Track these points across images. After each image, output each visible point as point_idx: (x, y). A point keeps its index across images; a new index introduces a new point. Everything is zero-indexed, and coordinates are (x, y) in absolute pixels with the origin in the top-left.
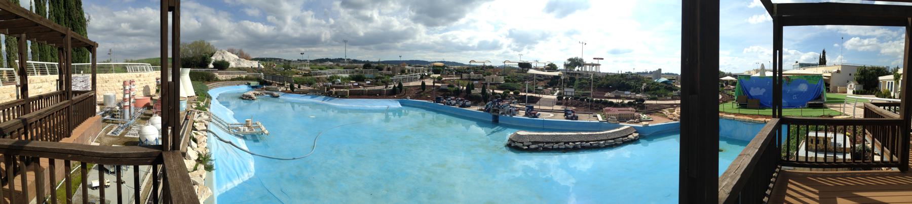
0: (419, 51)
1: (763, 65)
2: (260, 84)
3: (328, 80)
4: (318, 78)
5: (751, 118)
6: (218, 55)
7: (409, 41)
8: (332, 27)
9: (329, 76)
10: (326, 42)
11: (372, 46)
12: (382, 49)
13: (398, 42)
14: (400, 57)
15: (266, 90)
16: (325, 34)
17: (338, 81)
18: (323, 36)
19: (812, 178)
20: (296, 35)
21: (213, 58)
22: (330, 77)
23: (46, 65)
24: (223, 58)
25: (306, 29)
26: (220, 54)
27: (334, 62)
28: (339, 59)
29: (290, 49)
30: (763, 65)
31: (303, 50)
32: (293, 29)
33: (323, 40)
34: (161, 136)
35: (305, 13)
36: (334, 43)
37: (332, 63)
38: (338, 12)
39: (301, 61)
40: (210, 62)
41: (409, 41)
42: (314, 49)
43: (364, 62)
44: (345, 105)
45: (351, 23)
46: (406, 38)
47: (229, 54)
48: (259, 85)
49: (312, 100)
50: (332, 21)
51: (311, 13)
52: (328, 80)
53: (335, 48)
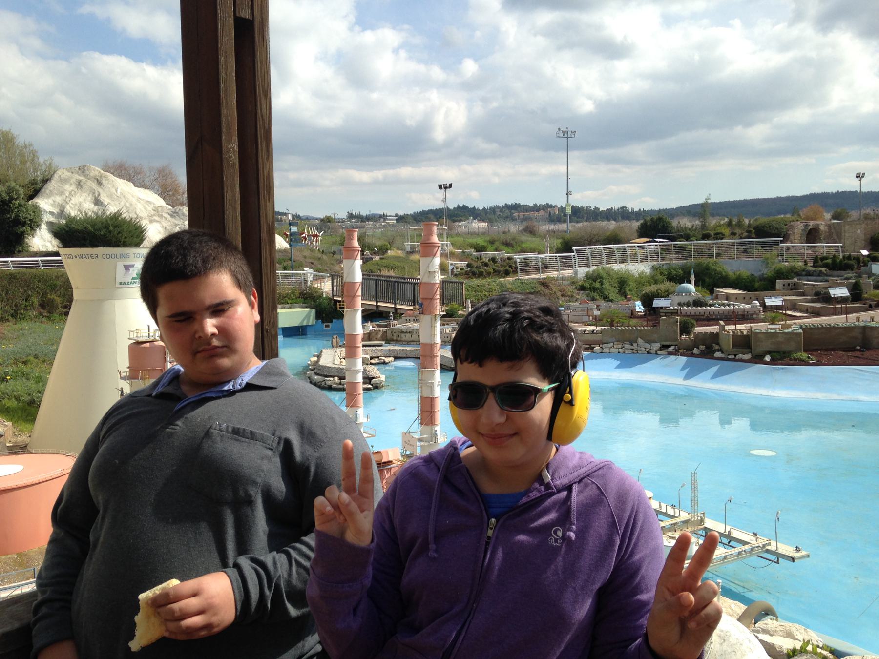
0: (845, 150)
1: (474, 206)
2: (319, 316)
3: (582, 288)
4: (544, 283)
5: (452, 638)
6: (68, 188)
7: (800, 115)
8: (469, 86)
9: (582, 272)
10: (449, 144)
11: (638, 150)
12: (679, 156)
13: (748, 124)
14: (860, 176)
15: (388, 341)
16: (447, 115)
17: (689, 293)
18: (439, 118)
19: (617, 527)
20: (332, 121)
21: (45, 204)
22: (588, 277)
23: (615, 250)
24: (97, 202)
25: (375, 96)
26: (79, 185)
27: (490, 221)
28: (507, 206)
29: (314, 175)
30: (474, 206)
31: (447, 175)
32: (318, 94)
33: (439, 135)
34: (741, 615)
35: (368, 37)
36: (482, 145)
37: (483, 225)
38: (494, 37)
39: (359, 217)
40: (33, 225)
41: (800, 115)
42: (405, 172)
43: (638, 215)
44: (820, 396)
45: (547, 68)
46: (785, 104)
47: (124, 186)
48: (312, 320)
49: (628, 376)
50: (470, 67)
51: (389, 36)
52: (582, 288)
53: (487, 168)
